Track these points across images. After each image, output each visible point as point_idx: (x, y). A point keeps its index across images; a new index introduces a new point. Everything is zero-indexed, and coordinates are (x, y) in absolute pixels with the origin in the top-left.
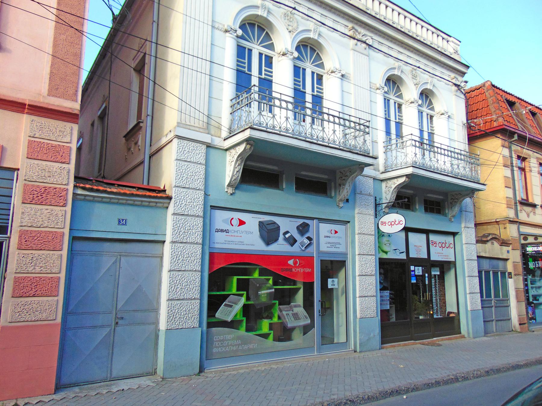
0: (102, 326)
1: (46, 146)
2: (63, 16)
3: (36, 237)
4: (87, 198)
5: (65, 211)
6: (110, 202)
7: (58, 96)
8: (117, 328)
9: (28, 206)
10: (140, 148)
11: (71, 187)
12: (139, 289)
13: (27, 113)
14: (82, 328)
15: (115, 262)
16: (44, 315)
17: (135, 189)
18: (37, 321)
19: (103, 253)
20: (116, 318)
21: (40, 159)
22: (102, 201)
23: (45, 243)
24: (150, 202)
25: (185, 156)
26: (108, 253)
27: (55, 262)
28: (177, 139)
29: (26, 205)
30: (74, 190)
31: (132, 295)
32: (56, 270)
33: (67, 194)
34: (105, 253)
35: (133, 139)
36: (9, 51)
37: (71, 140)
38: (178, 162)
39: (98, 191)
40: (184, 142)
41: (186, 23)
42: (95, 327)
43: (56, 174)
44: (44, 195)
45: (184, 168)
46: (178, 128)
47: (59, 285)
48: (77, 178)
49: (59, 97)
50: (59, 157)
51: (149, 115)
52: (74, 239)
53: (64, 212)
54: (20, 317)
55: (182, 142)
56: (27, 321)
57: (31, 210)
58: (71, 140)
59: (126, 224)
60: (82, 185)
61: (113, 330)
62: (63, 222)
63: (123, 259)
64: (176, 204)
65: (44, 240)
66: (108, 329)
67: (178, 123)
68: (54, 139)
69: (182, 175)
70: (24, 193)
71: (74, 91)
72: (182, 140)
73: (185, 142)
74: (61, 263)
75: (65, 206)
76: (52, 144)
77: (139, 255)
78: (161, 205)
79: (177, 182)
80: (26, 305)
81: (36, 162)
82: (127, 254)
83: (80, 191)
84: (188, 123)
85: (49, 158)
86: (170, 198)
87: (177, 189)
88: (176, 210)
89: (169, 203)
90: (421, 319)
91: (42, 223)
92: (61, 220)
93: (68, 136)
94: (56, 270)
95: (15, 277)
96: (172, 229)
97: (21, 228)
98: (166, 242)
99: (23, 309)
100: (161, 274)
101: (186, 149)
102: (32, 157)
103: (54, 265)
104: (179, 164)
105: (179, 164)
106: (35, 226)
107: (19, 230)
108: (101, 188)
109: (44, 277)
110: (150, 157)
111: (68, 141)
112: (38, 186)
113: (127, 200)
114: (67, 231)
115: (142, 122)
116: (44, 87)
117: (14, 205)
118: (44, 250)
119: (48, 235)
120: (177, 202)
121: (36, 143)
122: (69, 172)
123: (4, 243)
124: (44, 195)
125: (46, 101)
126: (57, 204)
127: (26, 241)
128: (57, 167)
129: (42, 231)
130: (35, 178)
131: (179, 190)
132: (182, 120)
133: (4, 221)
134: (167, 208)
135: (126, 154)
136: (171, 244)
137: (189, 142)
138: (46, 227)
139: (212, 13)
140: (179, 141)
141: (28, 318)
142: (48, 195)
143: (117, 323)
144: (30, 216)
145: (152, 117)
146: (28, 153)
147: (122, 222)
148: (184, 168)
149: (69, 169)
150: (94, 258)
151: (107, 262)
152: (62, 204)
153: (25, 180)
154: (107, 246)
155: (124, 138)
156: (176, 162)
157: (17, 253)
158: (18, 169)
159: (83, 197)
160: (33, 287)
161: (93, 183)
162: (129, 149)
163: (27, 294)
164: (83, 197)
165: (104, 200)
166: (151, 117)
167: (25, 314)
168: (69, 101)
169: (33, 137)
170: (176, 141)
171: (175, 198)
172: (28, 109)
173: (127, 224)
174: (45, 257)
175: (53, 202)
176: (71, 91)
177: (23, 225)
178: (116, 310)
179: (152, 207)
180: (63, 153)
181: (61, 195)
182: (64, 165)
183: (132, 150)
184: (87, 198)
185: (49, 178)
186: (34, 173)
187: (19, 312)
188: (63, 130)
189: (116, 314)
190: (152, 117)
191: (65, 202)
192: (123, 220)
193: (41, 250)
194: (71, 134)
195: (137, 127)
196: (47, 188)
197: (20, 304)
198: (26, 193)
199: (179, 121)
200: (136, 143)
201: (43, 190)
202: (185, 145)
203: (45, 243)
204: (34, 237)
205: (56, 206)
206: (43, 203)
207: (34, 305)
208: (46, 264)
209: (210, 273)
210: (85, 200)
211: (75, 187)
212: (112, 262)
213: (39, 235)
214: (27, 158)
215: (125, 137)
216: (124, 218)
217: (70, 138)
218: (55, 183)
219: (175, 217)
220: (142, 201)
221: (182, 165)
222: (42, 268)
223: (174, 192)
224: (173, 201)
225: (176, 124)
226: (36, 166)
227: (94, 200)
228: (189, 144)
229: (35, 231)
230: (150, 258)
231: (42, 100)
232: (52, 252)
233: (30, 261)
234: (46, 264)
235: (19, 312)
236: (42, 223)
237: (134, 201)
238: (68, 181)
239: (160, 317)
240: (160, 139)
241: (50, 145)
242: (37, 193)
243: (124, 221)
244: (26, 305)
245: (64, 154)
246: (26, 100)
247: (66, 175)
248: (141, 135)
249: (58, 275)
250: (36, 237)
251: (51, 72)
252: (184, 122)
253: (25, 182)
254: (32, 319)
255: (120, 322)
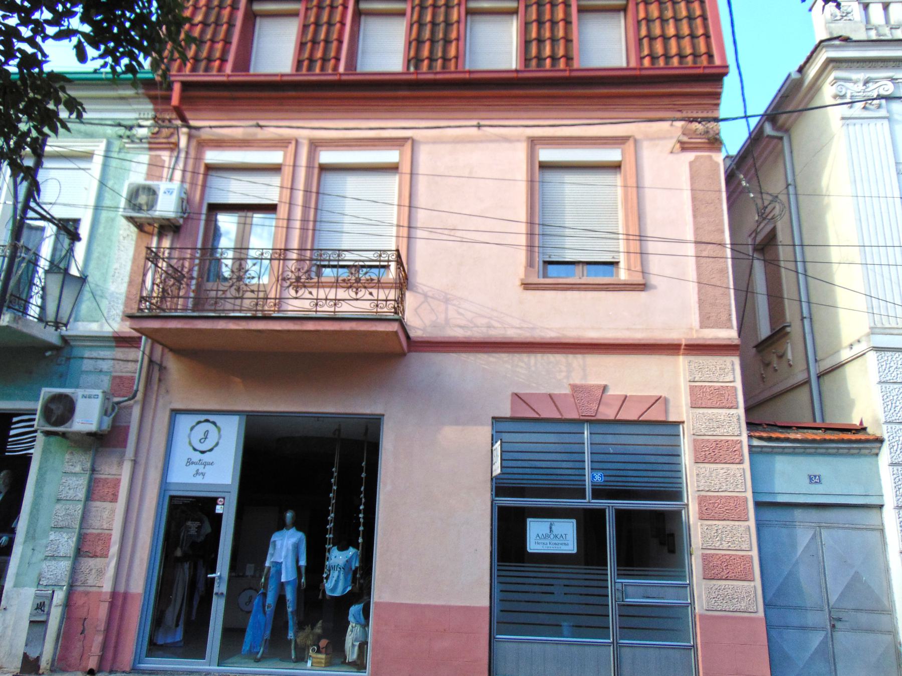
0: (814, 629)
1: (708, 390)
2: (737, 248)
3: (716, 505)
4: (764, 450)
5: (743, 469)
6: (793, 452)
7: (711, 325)
8: (834, 634)
9: (702, 465)
10: (791, 363)
11: (744, 438)
12: (856, 577)
13: (684, 354)
14: (787, 627)
15: (814, 537)
16: (743, 604)
17: (820, 431)
18: (736, 611)
19: (770, 522)
20: (831, 618)
21: (704, 406)
22: (783, 452)
23: (727, 511)
24: (849, 449)
25: (893, 375)
26: (802, 524)
27: (743, 536)
28: (875, 352)
29: (700, 465)
30: (748, 441)
31: (847, 587)
32: (746, 546)
33: (741, 447)
34: (797, 524)
35: (774, 351)
36: (654, 287)
37: (734, 378)
38: (884, 385)
39: (778, 440)
40: (887, 355)
41: (855, 181)
42: (803, 628)
43: (725, 423)
44: (717, 451)
45: (894, 393)
46: (873, 337)
47: (753, 566)
48: (750, 425)
49: (712, 327)
50: (725, 401)
51: (805, 318)
52: (758, 505)
53: (741, 471)
54: (716, 604)
55: (883, 355)
56: (725, 611)
57: (706, 471)
58: (734, 378)
59: (820, 481)
60: (757, 434)
61: (829, 635)
62: (743, 483)
63: (824, 533)
64: (892, 450)
65: (726, 508)
66: (823, 634)
67: (871, 328)
68: (716, 380)
69: (894, 405)
70: (695, 450)
71: (727, 315)
72: (883, 352)
73: (889, 354)
74: (750, 537)
75: (742, 463)
76: (715, 387)
77: (847, 526)
78: (867, 451)
79: (888, 416)
80: (720, 589)
81: (701, 411)
82: (829, 525)
83: (756, 443)
84: (887, 326)
85: (714, 405)
86: (880, 441)
87: (889, 426)
88: (895, 457)
89: (880, 448)
90: (110, 43)
91: (720, 486)
92: (741, 481)
93: (730, 373)
94: (746, 546)
95: (702, 553)
96: (894, 488)
97: (699, 493)
98: (885, 507)
99: (718, 595)
100: (886, 558)
101: (892, 364)
102: (696, 406)
103: (743, 539)
104: (886, 388)
105: (886, 388)
106: (712, 490)
107: (697, 495)
108: (774, 435)
109: (733, 555)
110: (819, 377)
111: (731, 379)
112: (708, 441)
113: (816, 448)
114: (749, 495)
115: (789, 326)
116: (694, 319)
117: (685, 465)
118: (728, 520)
119: (729, 501)
120: (893, 446)
121: (697, 389)
122: (739, 419)
123: (683, 512)
124: (717, 451)
125: (700, 336)
126: (732, 461)
127: (706, 509)
128: (724, 414)
129: (721, 496)
130: (703, 431)
131: (894, 428)
132: (876, 323)
133: (577, 472)
134: (877, 455)
135: (763, 372)
136: (897, 511)
137: (894, 353)
138: (725, 491)
139: (894, 154)
140: (878, 354)
141: (725, 606)
142: (721, 451)
143: (834, 626)
144: (706, 478)
145: (811, 319)
146: (691, 402)
147: (815, 479)
148: (894, 393)
149: (739, 415)
150: (784, 531)
151: (803, 537)
152: (737, 461)
153: (694, 434)
154: (798, 514)
155: (755, 349)
156: (879, 386)
157: (699, 524)
158: (683, 422)
159: (759, 449)
160: (724, 568)
161: (764, 428)
162: (767, 365)
163: (719, 575)
164: (759, 449)
165: (786, 450)
166: (809, 320)
167: (722, 601)
168: (724, 330)
169: (693, 381)
170: (872, 355)
171: (889, 440)
172: (684, 349)
173: (823, 481)
174: (730, 529)
175: (728, 458)
176: (724, 317)
177: (700, 489)
178: (829, 606)
179: (853, 455)
180: (729, 395)
181: (735, 449)
182: (732, 411)
183: (775, 366)
184: (764, 450)
185: (718, 429)
186: (702, 425)
187: (714, 598)
188: (723, 366)
189: (830, 612)
190: (811, 319)
191: (741, 458)
192: (815, 476)
193: (724, 520)
194: (733, 370)
195: (779, 333)
196: (718, 442)
197: (714, 588)
198: (697, 450)
199: (872, 325)
200: (781, 357)
201: (714, 444)
202: (890, 358)
203: (727, 511)
204: (715, 503)
205: (732, 463)
206: (717, 461)
207: (729, 591)
208: (734, 539)
209: (8, 558)
210: (761, 453)
211: (750, 437)
212: (810, 536)
213: (718, 501)
214: (692, 407)
215: (756, 347)
216: (817, 473)
217: (732, 376)
218: (726, 434)
219: (895, 468)
220: (838, 448)
221: (890, 389)
222: (730, 544)
223: (886, 432)
224: (888, 445)
225: (868, 330)
226: (702, 416)
227: (772, 452)
228: (895, 357)
229: (714, 497)
230: (864, 532)
231: (695, 336)
232: (737, 523)
233: (716, 534)
234: (734, 539)
235: (714, 598)
236: (720, 486)
237: (827, 448)
238: (740, 431)
239: (897, 623)
240: (838, 351)
241: (712, 388)
242: (707, 449)
243: (817, 477)
244: (720, 589)
245: (729, 397)
246: (680, 340)
247: (736, 423)
248: (789, 345)
249: (749, 553)
250: (716, 505)
251: (700, 300)
252: (879, 325)
253: (693, 437)
254: (730, 608)
255: (839, 625)
